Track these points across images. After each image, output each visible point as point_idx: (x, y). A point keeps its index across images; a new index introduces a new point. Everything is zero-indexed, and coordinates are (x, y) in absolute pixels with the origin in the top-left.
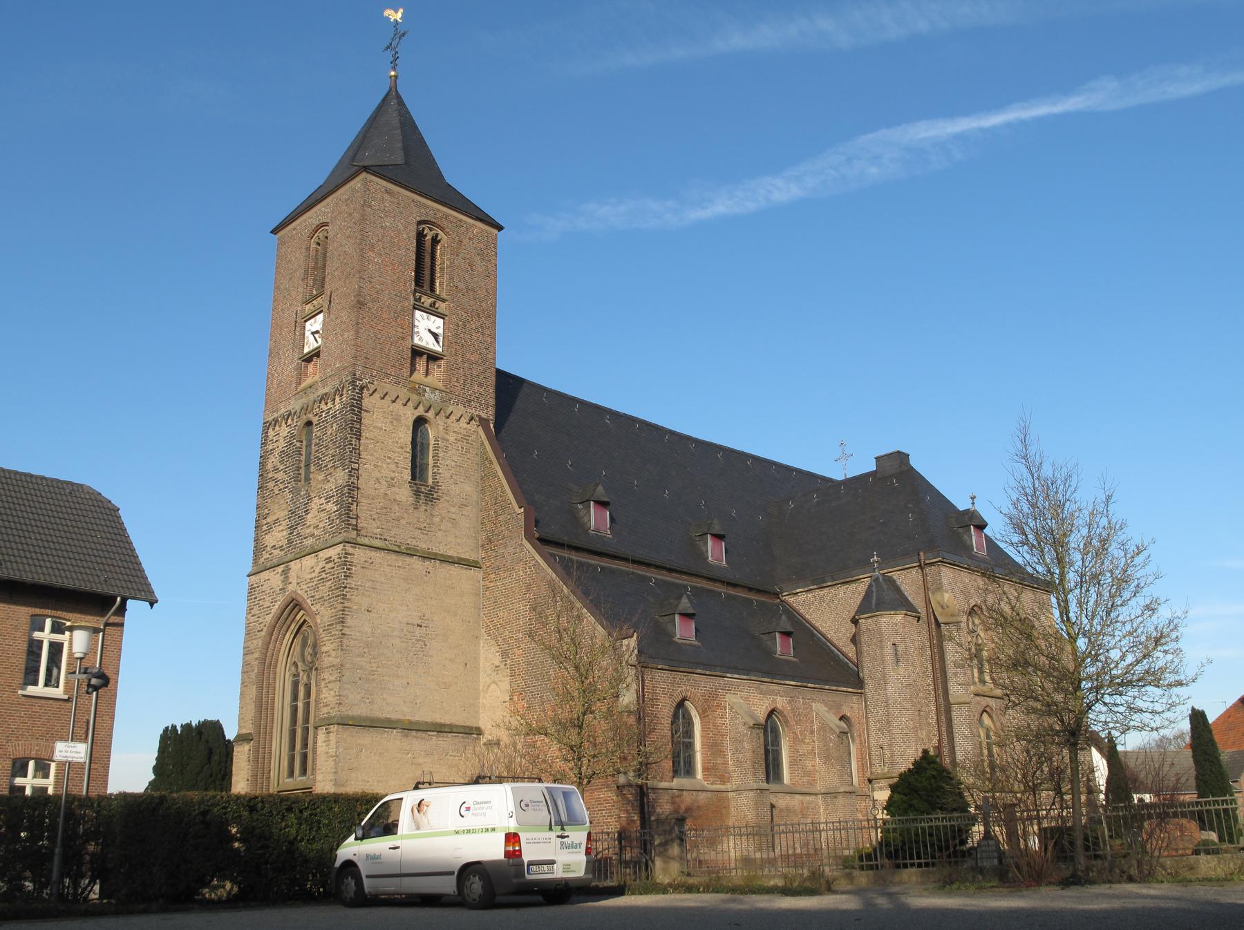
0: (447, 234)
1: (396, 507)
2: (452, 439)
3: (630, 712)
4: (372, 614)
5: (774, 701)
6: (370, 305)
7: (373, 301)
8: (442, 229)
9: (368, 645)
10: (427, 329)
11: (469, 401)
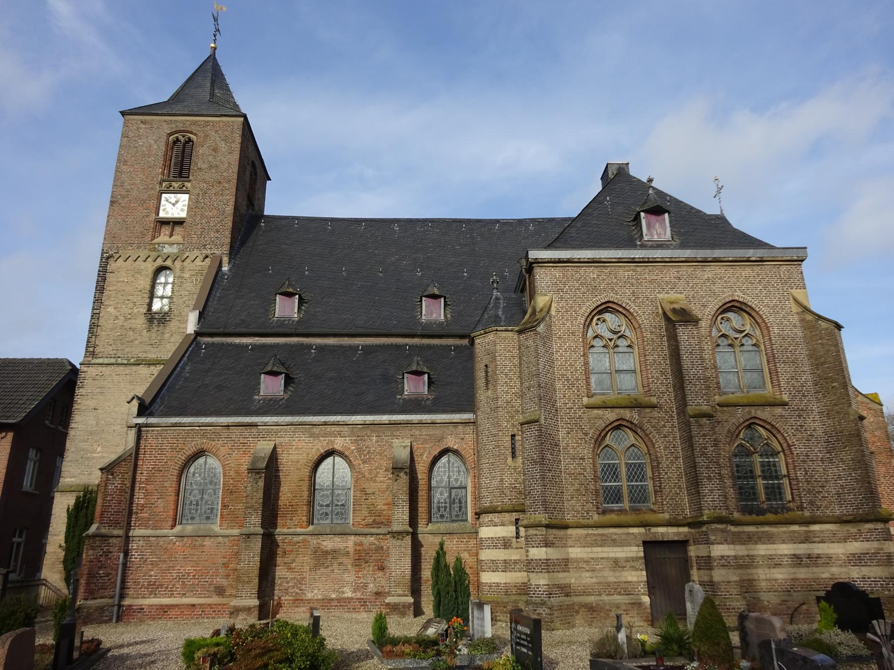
0: (195, 134)
1: (131, 333)
2: (187, 275)
3: (874, 507)
4: (98, 411)
5: (333, 442)
6: (121, 201)
7: (123, 197)
8: (191, 133)
9: (91, 433)
10: (175, 206)
11: (206, 245)
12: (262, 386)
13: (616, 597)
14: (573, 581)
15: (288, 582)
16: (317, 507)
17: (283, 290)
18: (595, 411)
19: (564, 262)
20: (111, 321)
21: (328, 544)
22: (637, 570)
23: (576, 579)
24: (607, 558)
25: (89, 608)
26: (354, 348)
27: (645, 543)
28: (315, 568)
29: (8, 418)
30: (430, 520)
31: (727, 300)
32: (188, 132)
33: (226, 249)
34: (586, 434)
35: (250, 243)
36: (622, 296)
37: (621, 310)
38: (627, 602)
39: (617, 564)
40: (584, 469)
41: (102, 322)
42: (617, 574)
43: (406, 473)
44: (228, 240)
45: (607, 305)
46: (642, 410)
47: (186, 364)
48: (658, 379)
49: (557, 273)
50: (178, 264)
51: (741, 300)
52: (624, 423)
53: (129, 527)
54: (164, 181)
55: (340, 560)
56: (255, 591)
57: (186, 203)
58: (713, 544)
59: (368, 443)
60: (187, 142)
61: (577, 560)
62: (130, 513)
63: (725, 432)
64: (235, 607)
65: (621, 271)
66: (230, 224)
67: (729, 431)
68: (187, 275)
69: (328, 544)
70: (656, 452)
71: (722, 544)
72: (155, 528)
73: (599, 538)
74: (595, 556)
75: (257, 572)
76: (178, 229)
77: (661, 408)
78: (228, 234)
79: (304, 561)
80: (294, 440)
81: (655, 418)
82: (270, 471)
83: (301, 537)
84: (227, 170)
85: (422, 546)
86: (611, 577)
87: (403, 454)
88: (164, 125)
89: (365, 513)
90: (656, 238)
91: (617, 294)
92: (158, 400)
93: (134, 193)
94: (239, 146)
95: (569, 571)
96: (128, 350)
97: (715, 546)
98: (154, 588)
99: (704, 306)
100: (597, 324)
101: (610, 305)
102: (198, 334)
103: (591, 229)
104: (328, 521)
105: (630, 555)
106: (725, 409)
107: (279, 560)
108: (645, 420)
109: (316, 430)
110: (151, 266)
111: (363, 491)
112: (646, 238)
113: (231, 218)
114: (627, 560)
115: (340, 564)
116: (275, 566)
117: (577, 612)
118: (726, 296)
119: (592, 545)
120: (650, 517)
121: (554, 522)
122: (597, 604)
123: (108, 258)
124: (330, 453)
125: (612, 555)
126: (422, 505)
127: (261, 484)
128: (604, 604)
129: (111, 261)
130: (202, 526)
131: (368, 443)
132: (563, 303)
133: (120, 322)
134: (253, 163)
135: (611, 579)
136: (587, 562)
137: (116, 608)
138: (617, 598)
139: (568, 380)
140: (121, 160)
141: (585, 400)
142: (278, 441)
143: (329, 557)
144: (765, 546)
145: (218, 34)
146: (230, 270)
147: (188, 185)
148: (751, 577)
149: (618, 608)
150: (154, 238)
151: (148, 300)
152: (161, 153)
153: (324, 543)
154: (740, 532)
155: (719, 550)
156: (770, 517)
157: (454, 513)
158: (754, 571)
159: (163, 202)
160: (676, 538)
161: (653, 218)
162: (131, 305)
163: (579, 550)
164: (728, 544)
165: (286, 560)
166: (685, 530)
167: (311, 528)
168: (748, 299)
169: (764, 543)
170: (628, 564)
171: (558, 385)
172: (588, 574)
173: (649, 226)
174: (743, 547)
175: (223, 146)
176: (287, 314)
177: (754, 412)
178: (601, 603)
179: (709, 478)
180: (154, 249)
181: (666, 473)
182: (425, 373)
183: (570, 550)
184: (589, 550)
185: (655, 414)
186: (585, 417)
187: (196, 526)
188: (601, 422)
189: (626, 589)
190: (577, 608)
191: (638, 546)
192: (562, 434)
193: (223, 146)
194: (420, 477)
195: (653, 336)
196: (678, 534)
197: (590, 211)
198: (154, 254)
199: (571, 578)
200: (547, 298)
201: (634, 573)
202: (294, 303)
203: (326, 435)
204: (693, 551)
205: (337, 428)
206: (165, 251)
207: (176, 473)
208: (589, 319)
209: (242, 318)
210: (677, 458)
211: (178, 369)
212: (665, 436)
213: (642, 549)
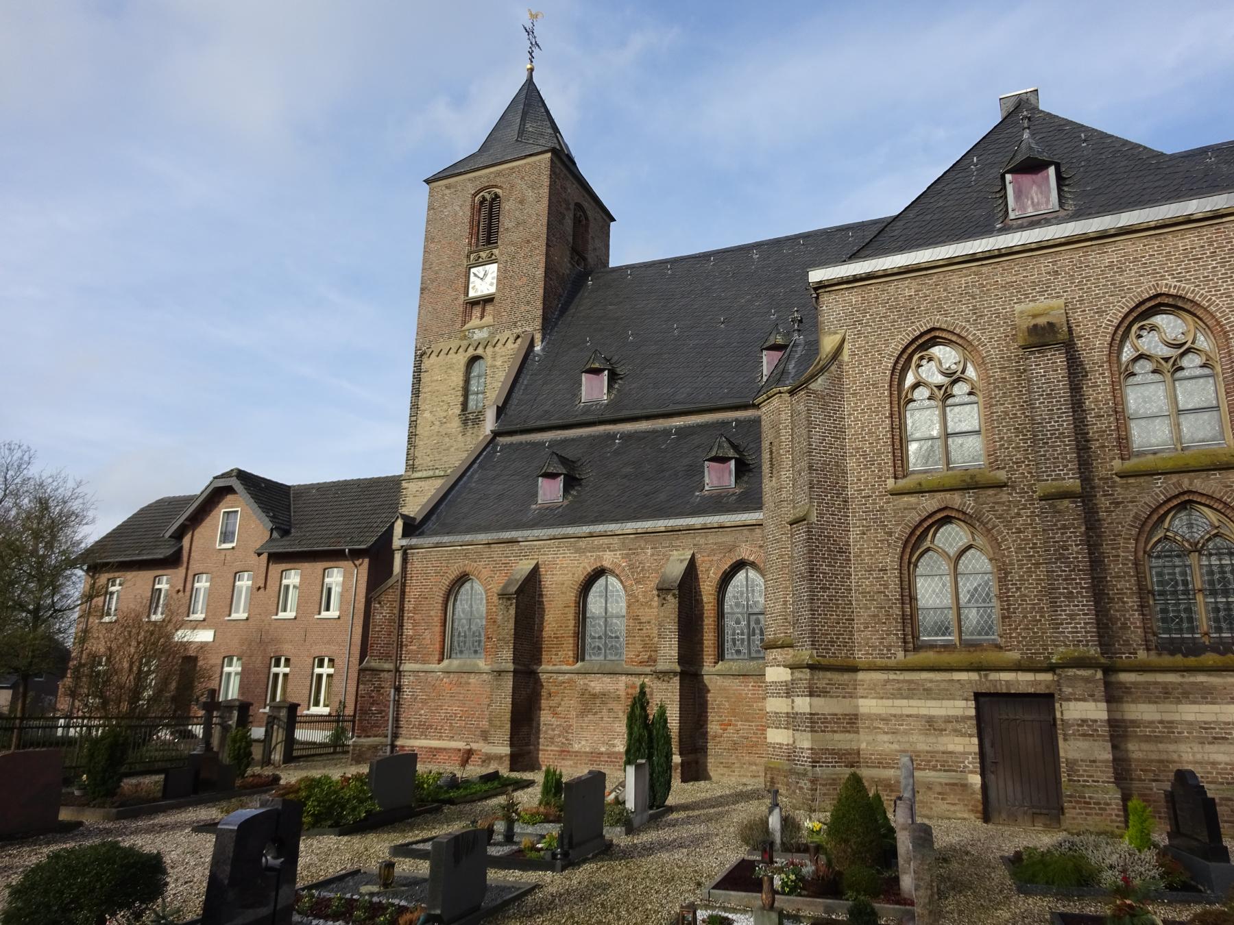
0: (500, 187)
2: (498, 363)
8: (496, 186)
10: (484, 281)
12: (540, 492)
14: (863, 746)
15: (553, 730)
16: (588, 640)
17: (771, 342)
18: (906, 499)
19: (862, 279)
20: (427, 428)
21: (598, 685)
22: (963, 735)
24: (917, 716)
25: (362, 746)
26: (666, 432)
27: (978, 696)
28: (582, 714)
29: (361, 543)
30: (720, 656)
31: (1146, 296)
32: (493, 186)
33: (538, 324)
34: (890, 534)
35: (572, 311)
36: (955, 317)
37: (954, 338)
38: (947, 781)
39: (931, 725)
40: (886, 586)
41: (419, 430)
42: (932, 739)
43: (674, 595)
44: (540, 312)
45: (933, 334)
46: (981, 491)
47: (476, 472)
48: (1010, 441)
49: (853, 297)
50: (489, 350)
51: (1173, 291)
53: (399, 659)
54: (471, 253)
55: (610, 706)
56: (507, 737)
57: (495, 275)
58: (1069, 700)
59: (642, 557)
60: (493, 200)
61: (870, 717)
62: (401, 646)
63: (1129, 519)
64: (486, 754)
65: (955, 279)
66: (541, 291)
67: (1136, 517)
68: (498, 363)
69: (598, 685)
71: (1084, 700)
72: (424, 662)
73: (905, 686)
74: (898, 712)
75: (508, 716)
76: (489, 308)
77: (1013, 488)
78: (539, 304)
79: (570, 705)
80: (561, 561)
81: (1003, 503)
82: (527, 597)
83: (567, 676)
84: (535, 225)
85: (708, 691)
86: (922, 743)
87: (675, 569)
88: (467, 185)
89: (639, 647)
90: (1030, 211)
91: (946, 315)
92: (434, 518)
93: (443, 274)
94: (547, 191)
95: (857, 732)
96: (445, 459)
97: (1072, 704)
98: (425, 729)
99: (1100, 312)
100: (1140, 336)
101: (937, 333)
102: (496, 434)
103: (928, 217)
104: (602, 657)
105: (951, 712)
106: (1131, 480)
107: (544, 703)
108: (986, 507)
109: (582, 544)
110: (461, 359)
111: (636, 618)
112: (1012, 215)
113: (542, 284)
114: (948, 720)
115: (610, 710)
116: (540, 709)
118: (1145, 289)
119: (894, 696)
120: (992, 657)
121: (824, 662)
123: (422, 355)
124: (740, 565)
125: (923, 711)
126: (709, 638)
127: (512, 611)
129: (425, 358)
130: (468, 661)
131: (642, 557)
132: (861, 342)
133: (436, 428)
134: (579, 206)
135: (922, 747)
136: (885, 720)
137: (389, 748)
139: (865, 455)
140: (429, 239)
141: (891, 483)
142: (541, 559)
143: (598, 701)
144: (1195, 708)
145: (536, 50)
146: (543, 350)
147: (496, 251)
148: (1164, 757)
149: (930, 789)
150: (464, 323)
151: (461, 399)
152: (467, 220)
153: (592, 684)
154: (1148, 683)
156: (1210, 658)
157: (753, 649)
159: (472, 278)
160: (1032, 690)
161: (1026, 179)
162: (445, 407)
163: (873, 702)
164: (1095, 701)
165: (552, 703)
166: (1047, 677)
167: (579, 664)
168: (1187, 289)
169: (1194, 703)
170: (950, 726)
171: (851, 464)
172: (886, 738)
173: (1019, 195)
174: (1153, 707)
175: (530, 194)
176: (595, 397)
177: (1185, 482)
180: (465, 337)
181: (1018, 589)
182: (730, 459)
183: (861, 702)
184: (889, 703)
185: (1004, 496)
187: (462, 661)
188: (914, 513)
189: (946, 762)
191: (966, 700)
192: (853, 535)
193: (530, 194)
194: (705, 600)
195: (1006, 374)
196: (1035, 683)
197: (939, 187)
198: (465, 343)
199: (863, 742)
200: (838, 338)
201: (958, 740)
202: (602, 381)
203: (592, 550)
205: (606, 540)
206: (476, 337)
207: (440, 600)
208: (902, 361)
209: (546, 408)
211: (465, 479)
213: (972, 704)
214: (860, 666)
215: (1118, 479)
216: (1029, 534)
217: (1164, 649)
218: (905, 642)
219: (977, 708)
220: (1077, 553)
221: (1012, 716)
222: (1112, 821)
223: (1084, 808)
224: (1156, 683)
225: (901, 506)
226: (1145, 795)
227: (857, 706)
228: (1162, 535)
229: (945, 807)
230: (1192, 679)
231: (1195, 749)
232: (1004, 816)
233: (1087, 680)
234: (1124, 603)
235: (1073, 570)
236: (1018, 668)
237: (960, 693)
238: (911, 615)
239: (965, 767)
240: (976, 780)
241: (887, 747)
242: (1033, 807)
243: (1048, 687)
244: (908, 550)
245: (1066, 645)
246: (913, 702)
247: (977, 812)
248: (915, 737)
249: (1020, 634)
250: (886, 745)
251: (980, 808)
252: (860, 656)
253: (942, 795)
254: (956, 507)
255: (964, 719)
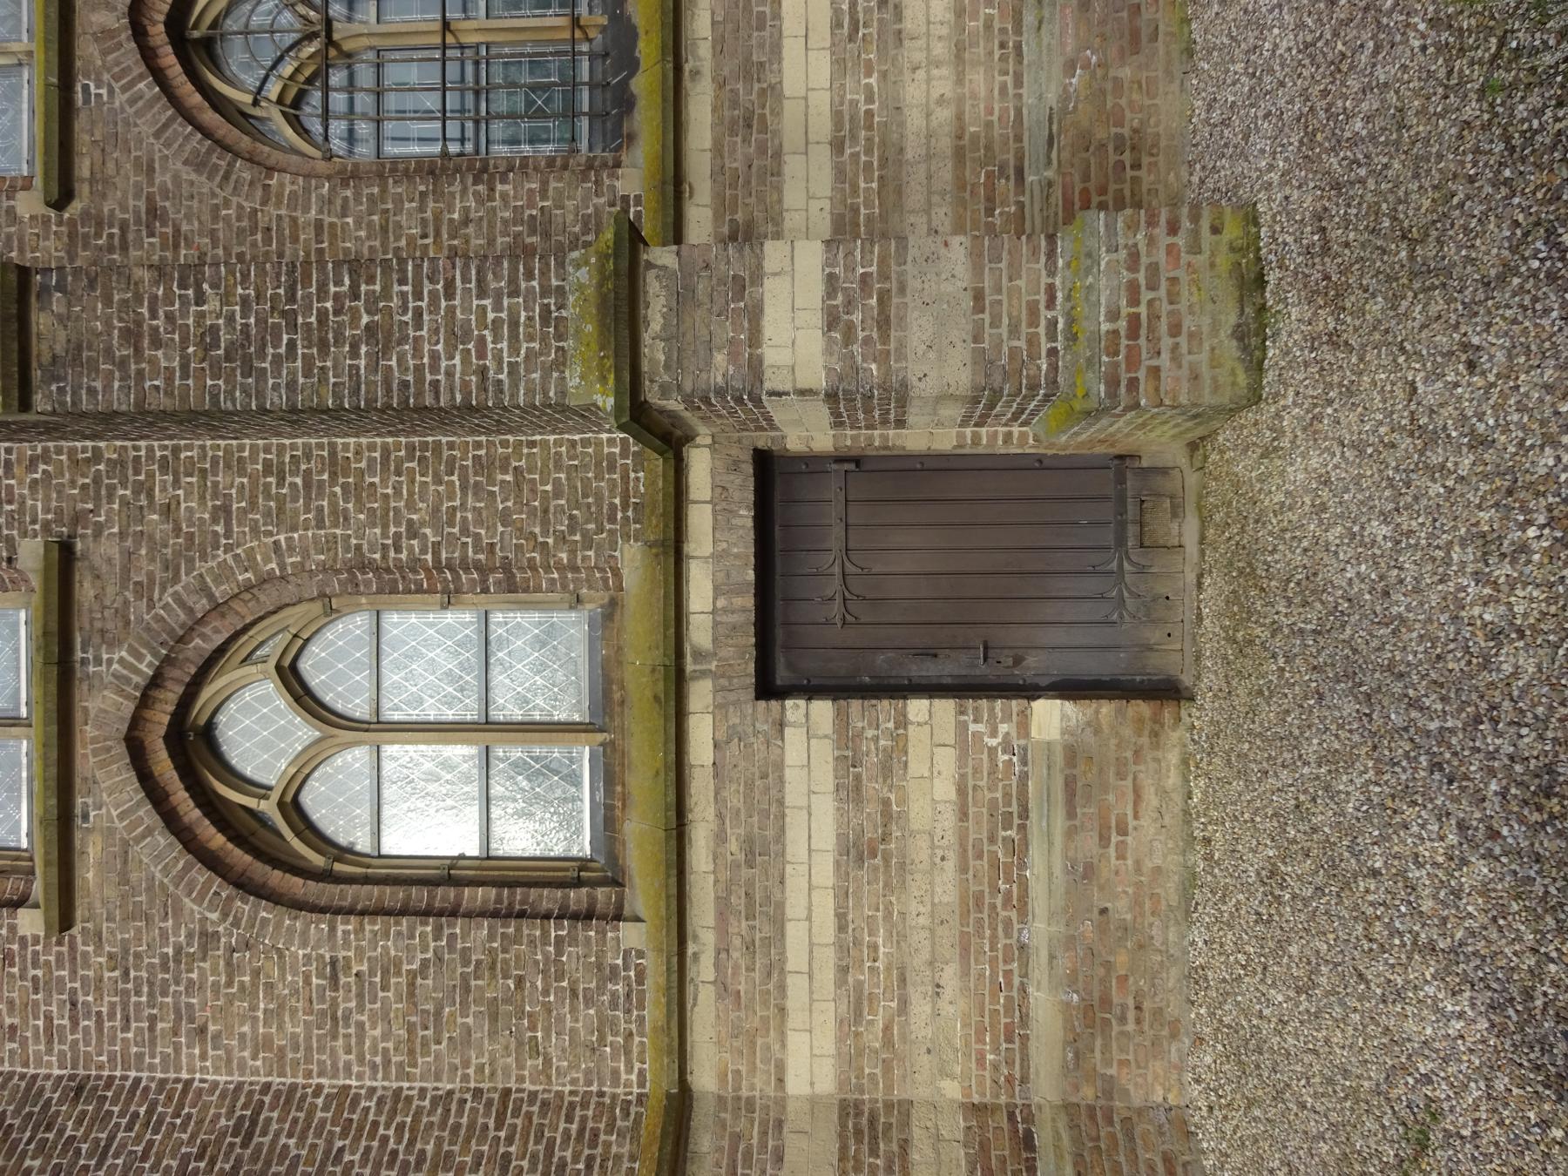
13: (1036, 870)
14: (952, 1090)
18: (88, 874)
22: (900, 744)
23: (944, 1073)
24: (842, 894)
27: (767, 688)
38: (1060, 822)
39: (868, 850)
40: (389, 967)
42: (920, 851)
52: (161, 718)
58: (756, 367)
61: (850, 1058)
63: (204, 184)
67: (198, 163)
70: (300, 568)
71: (755, 313)
73: (739, 926)
74: (827, 960)
77: (78, 519)
81: (129, 555)
86: (936, 887)
97: (773, 355)
105: (825, 776)
106: (83, 168)
114: (850, 791)
117: (1109, 1088)
119: (776, 969)
122: (1072, 981)
128: (1070, 942)
135: (947, 888)
136: (857, 1007)
138: (1044, 868)
144: (792, 49)
148: (945, 144)
149: (1089, 871)
154: (718, 172)
155: (794, 337)
158: (915, 120)
164: (758, 276)
166: (701, 465)
169: (776, 50)
170: (873, 787)
172: (920, 1008)
174: (793, 165)
178: (1064, 963)
179: (381, 337)
181: (413, 533)
183: (796, 1085)
184: (797, 988)
186: (116, 935)
190: (1088, 1093)
191: (781, 725)
201: (917, 766)
204: (807, 431)
210: (336, 466)
212: (223, 512)
213: (795, 708)
214: (670, 1085)
215: (76, 208)
216: (232, 484)
217: (617, 132)
218: (588, 916)
219: (811, 691)
220: (226, 299)
221: (834, 586)
222: (1195, 249)
223: (1153, 338)
224: (717, 150)
225: (111, 892)
226: (1068, 204)
227: (814, 1101)
228: (275, 114)
229: (1147, 822)
230: (704, 51)
231: (919, 56)
232: (1155, 635)
233: (683, 298)
234: (466, 221)
235: (291, 317)
236: (672, 550)
237: (758, 744)
238: (499, 883)
239: (1007, 747)
240: (1050, 718)
241: (954, 1006)
242: (1121, 541)
243: (735, 466)
244: (276, 878)
245: (561, 363)
246: (795, 905)
247: (1157, 719)
248: (914, 907)
249: (562, 539)
250: (948, 1010)
251: (1143, 708)
252: (636, 1075)
253: (1110, 830)
254: (129, 708)
255: (845, 736)
